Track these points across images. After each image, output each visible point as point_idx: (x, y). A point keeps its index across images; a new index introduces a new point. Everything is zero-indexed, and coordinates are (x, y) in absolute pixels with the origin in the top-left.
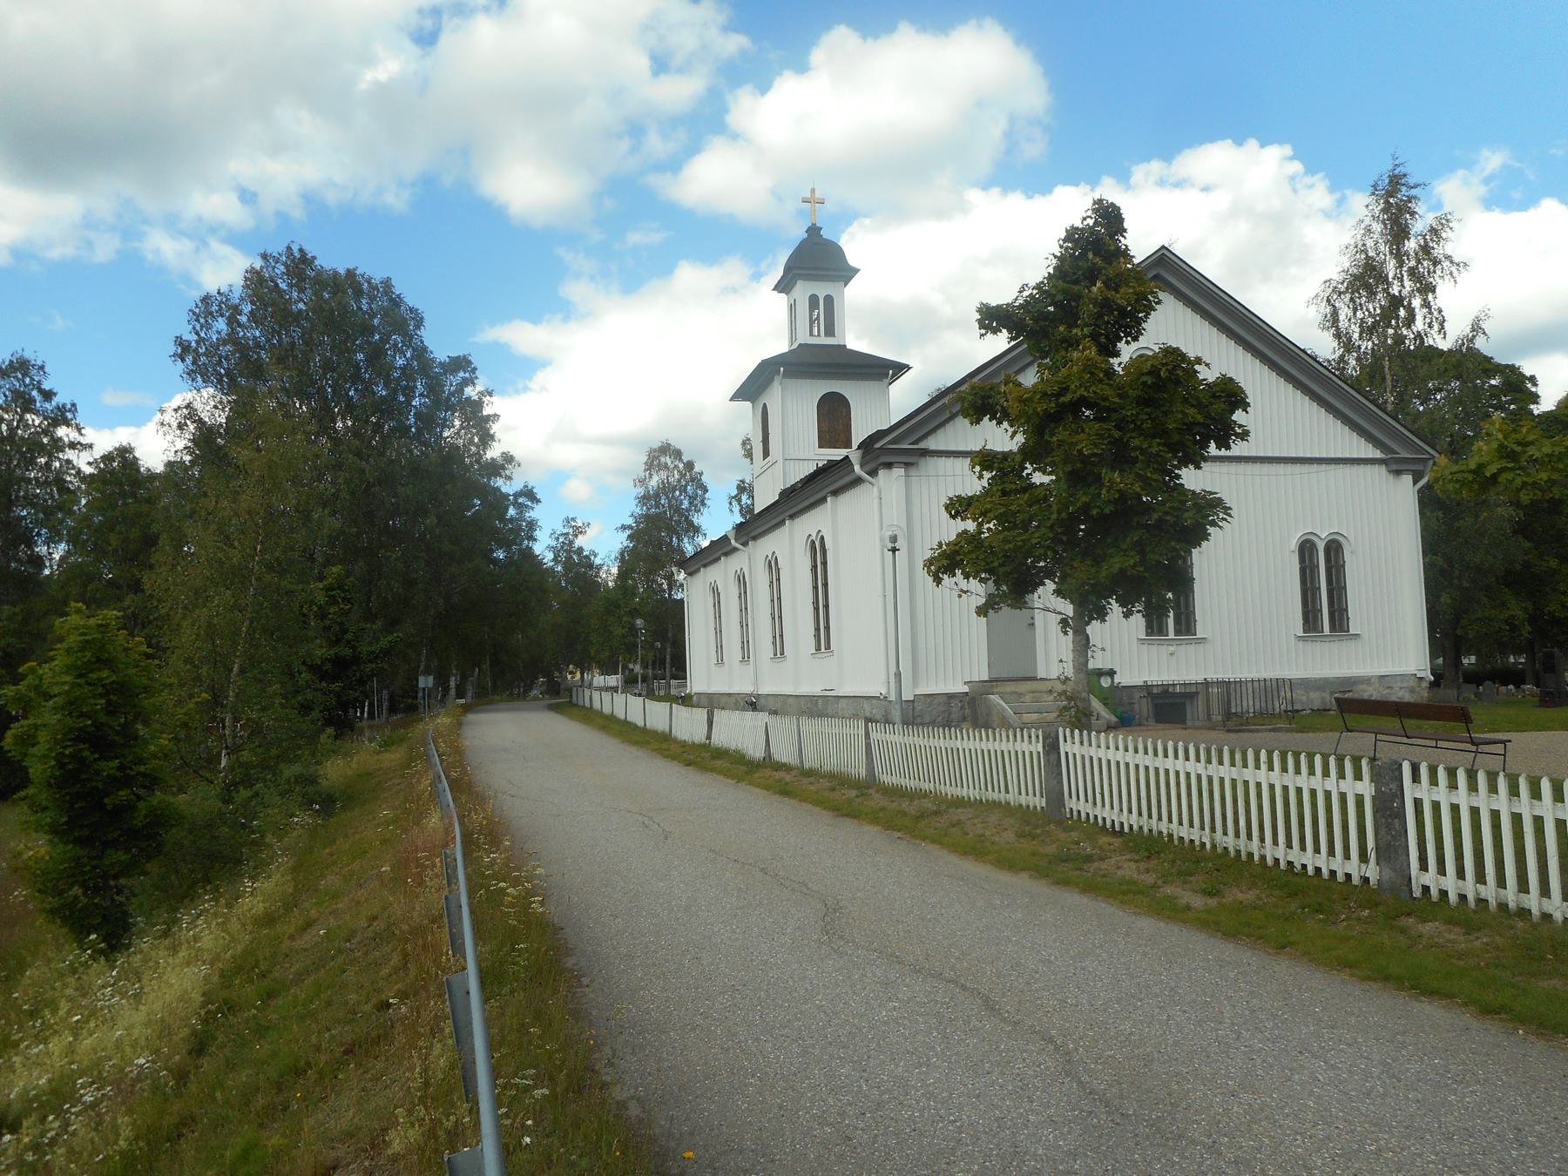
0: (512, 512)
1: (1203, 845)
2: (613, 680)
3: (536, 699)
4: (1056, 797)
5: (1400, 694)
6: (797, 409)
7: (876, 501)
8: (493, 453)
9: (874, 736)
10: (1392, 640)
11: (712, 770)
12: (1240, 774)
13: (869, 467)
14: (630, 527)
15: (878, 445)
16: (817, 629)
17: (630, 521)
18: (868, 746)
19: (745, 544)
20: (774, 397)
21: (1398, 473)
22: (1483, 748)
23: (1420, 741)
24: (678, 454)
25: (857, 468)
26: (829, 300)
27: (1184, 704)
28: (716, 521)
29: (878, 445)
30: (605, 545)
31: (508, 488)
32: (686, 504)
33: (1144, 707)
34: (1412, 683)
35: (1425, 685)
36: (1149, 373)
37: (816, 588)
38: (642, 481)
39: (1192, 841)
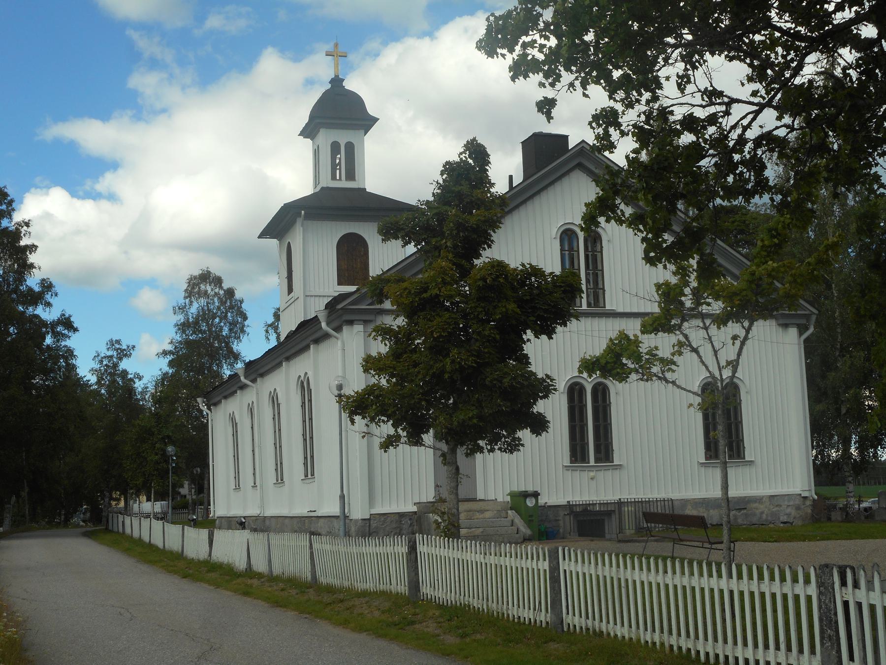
0: (49, 340)
1: (654, 644)
2: (158, 506)
3: (77, 526)
4: (414, 585)
5: (787, 513)
6: (318, 252)
7: (340, 352)
8: (33, 281)
9: (315, 546)
10: (780, 462)
11: (201, 580)
12: (499, 561)
13: (336, 324)
14: (170, 352)
15: (340, 306)
16: (306, 458)
17: (170, 348)
18: (312, 554)
19: (254, 381)
20: (297, 238)
21: (785, 326)
22: (714, 546)
23: (688, 543)
24: (218, 281)
25: (324, 325)
26: (350, 147)
27: (603, 520)
28: (253, 345)
29: (340, 306)
30: (148, 367)
31: (47, 315)
32: (225, 331)
33: (566, 523)
34: (798, 502)
35: (808, 503)
36: (480, 280)
37: (304, 421)
38: (182, 309)
39: (689, 650)
